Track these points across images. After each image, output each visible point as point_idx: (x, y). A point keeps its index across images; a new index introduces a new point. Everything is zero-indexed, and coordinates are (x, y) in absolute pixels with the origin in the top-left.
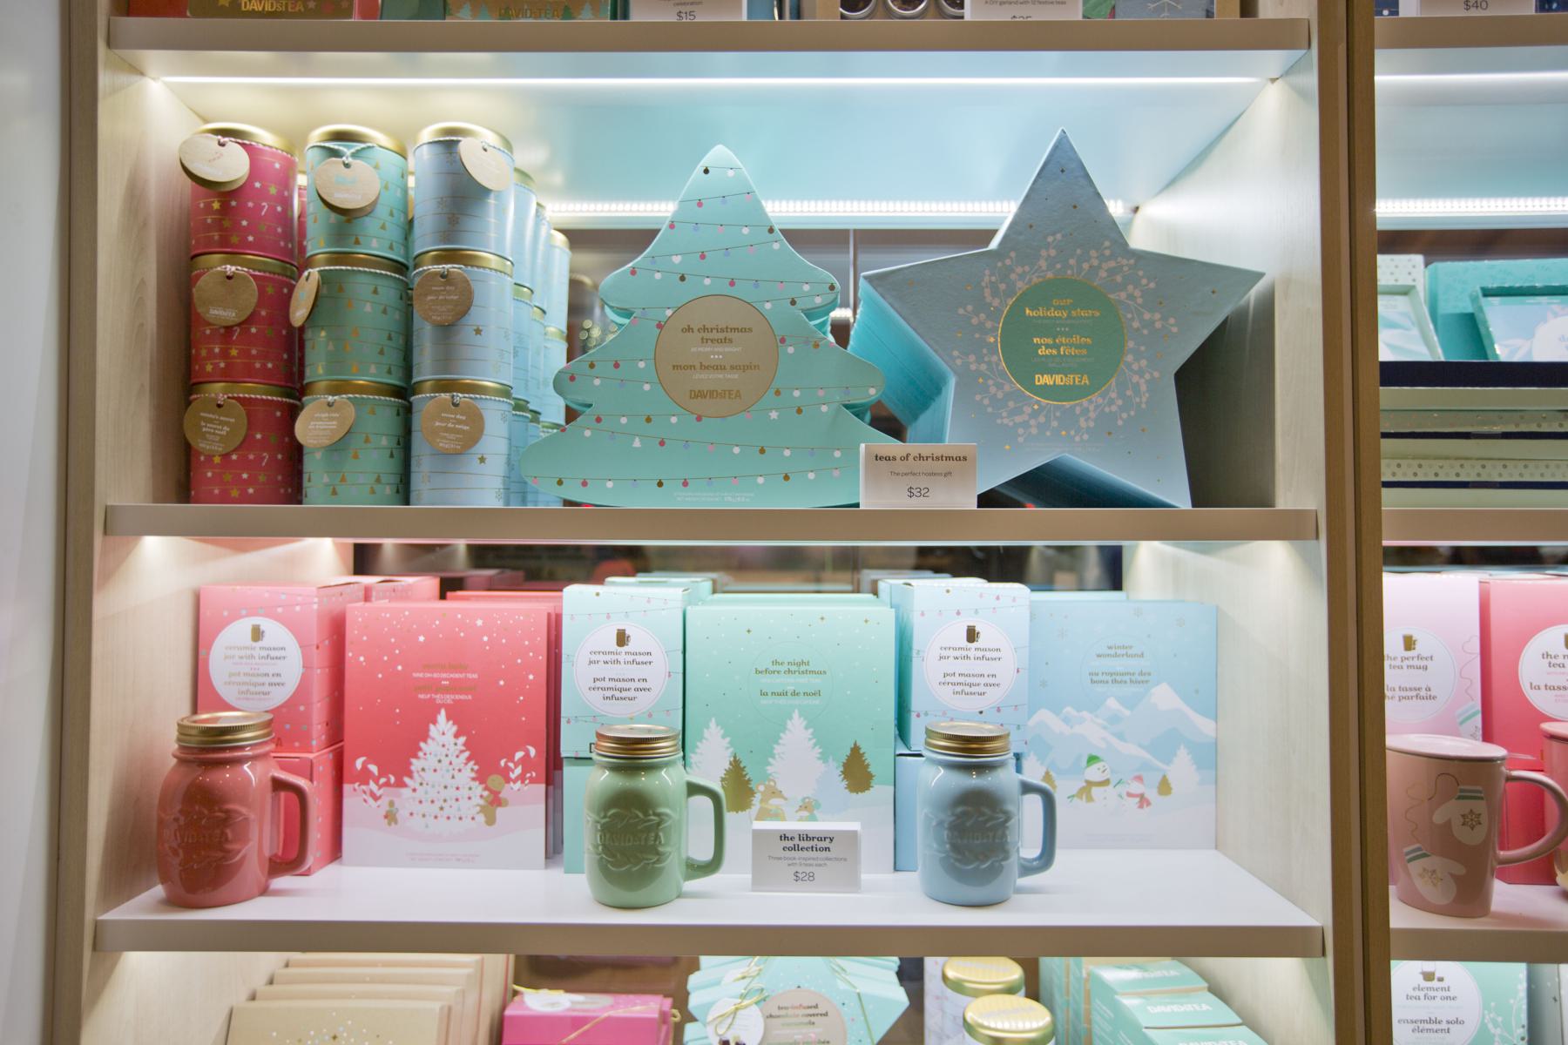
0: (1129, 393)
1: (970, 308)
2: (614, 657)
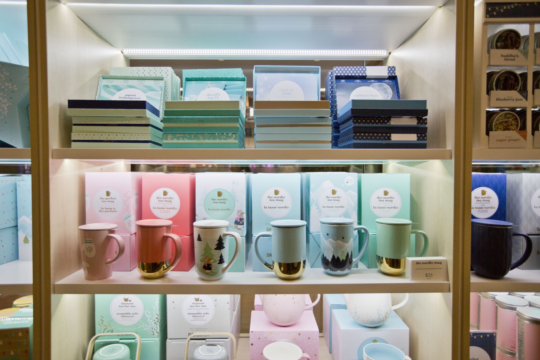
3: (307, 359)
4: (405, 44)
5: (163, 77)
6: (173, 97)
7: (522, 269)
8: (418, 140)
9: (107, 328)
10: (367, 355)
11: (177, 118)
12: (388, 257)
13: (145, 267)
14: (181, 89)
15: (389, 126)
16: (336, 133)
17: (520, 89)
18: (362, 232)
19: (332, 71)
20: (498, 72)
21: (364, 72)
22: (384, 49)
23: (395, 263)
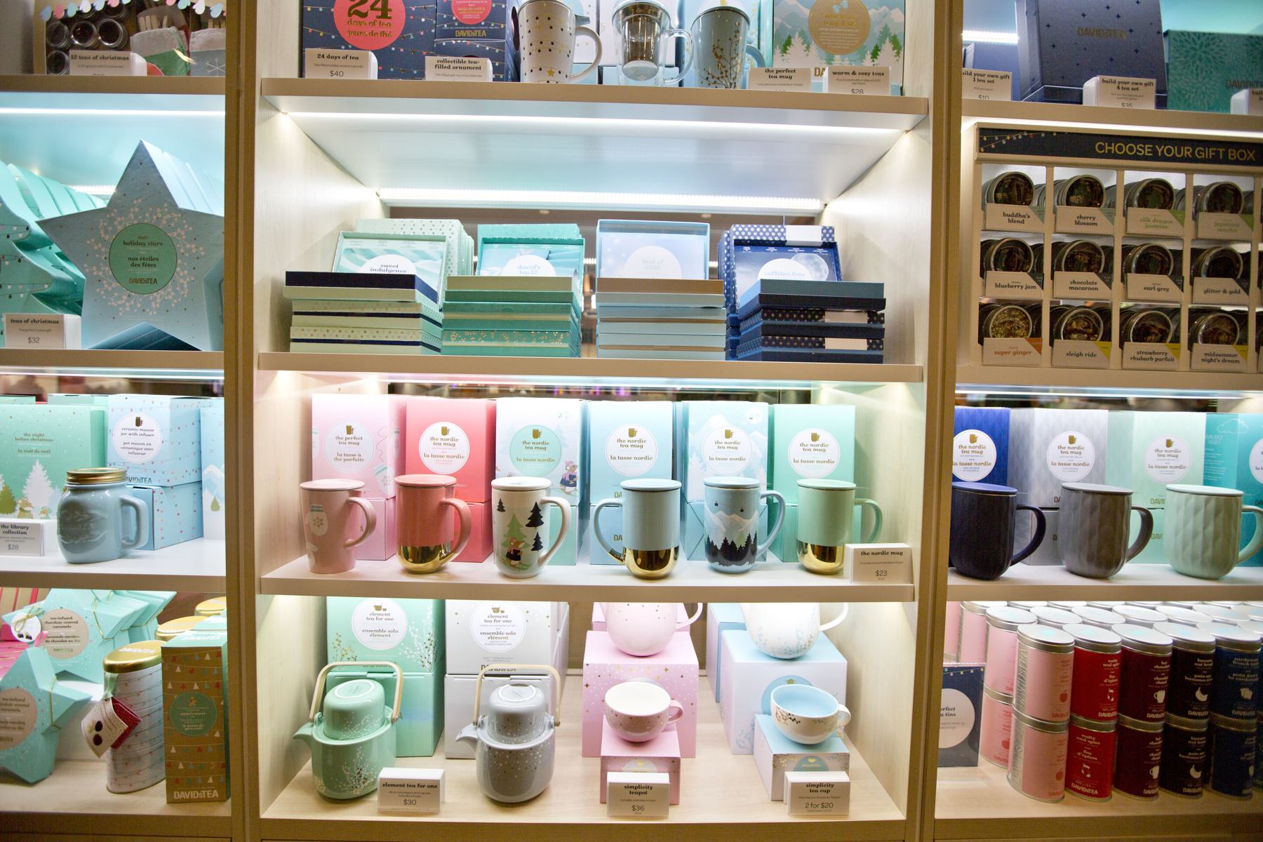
0: (178, 289)
1: (93, 240)
2: (134, 432)
3: (678, 710)
4: (851, 190)
5: (445, 237)
6: (460, 269)
7: (1029, 565)
8: (868, 349)
9: (347, 654)
10: (776, 704)
11: (466, 304)
12: (816, 544)
13: (410, 555)
14: (476, 259)
15: (823, 325)
16: (733, 335)
17: (1033, 271)
18: (774, 502)
19: (728, 232)
20: (999, 241)
21: (782, 235)
22: (816, 198)
23: (827, 553)
